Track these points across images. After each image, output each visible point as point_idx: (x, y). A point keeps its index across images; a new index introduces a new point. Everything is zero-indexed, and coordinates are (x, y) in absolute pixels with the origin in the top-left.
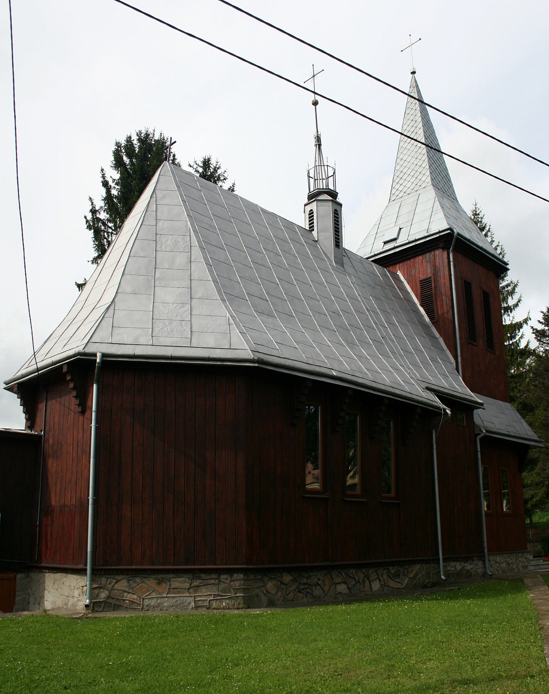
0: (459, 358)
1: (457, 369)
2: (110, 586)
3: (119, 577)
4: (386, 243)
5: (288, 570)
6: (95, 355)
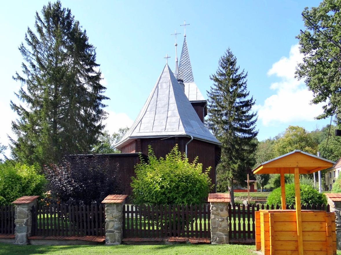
6: (190, 136)
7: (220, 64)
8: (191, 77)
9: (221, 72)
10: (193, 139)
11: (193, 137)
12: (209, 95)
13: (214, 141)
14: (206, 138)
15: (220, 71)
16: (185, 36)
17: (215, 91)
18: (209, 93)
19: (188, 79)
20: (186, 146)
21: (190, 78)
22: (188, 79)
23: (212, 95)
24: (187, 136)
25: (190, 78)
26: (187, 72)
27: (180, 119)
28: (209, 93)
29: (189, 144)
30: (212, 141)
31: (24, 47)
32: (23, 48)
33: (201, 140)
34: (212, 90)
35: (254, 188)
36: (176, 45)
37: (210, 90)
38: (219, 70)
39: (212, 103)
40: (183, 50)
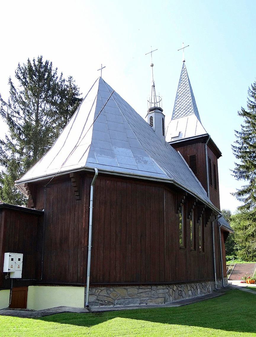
0: (209, 192)
1: (208, 196)
2: (98, 293)
3: (103, 288)
4: (172, 138)
5: (175, 284)
6: (94, 170)
7: (251, 94)
8: (190, 108)
9: (252, 104)
10: (97, 174)
11: (99, 170)
12: (238, 135)
13: (152, 176)
14: (131, 172)
15: (250, 102)
16: (184, 61)
17: (247, 129)
18: (237, 132)
19: (187, 111)
20: (92, 187)
21: (189, 109)
22: (187, 111)
23: (243, 135)
24: (87, 170)
25: (189, 109)
26: (186, 103)
27: (89, 146)
28: (237, 132)
29: (95, 182)
30: (112, 170)
31: (3, 109)
32: (3, 110)
33: (121, 175)
34: (243, 129)
35: (31, 285)
36: (152, 66)
37: (241, 130)
38: (249, 102)
39: (243, 145)
40: (181, 78)
